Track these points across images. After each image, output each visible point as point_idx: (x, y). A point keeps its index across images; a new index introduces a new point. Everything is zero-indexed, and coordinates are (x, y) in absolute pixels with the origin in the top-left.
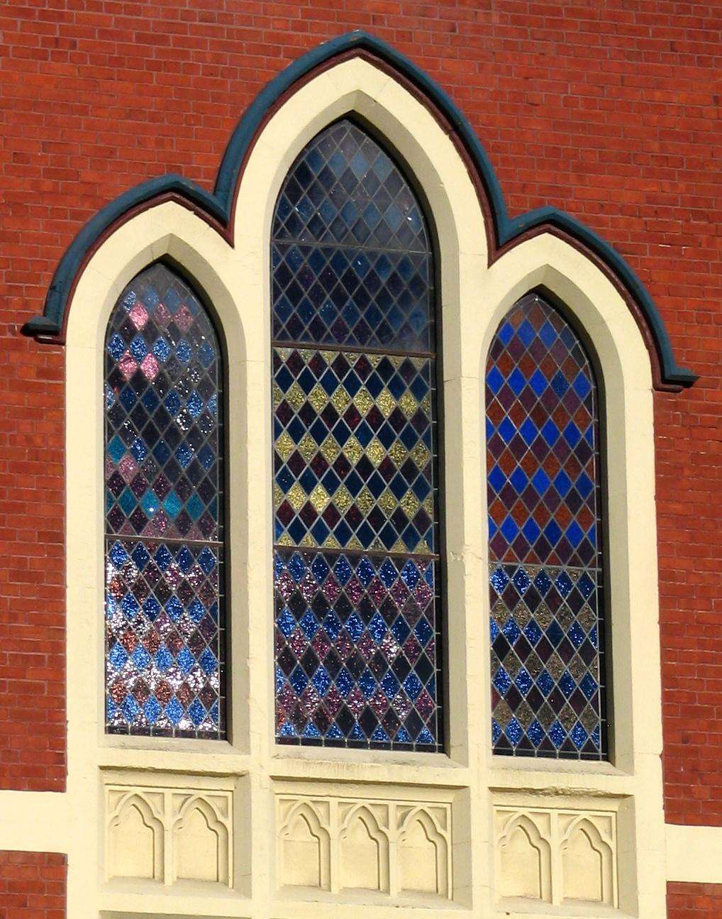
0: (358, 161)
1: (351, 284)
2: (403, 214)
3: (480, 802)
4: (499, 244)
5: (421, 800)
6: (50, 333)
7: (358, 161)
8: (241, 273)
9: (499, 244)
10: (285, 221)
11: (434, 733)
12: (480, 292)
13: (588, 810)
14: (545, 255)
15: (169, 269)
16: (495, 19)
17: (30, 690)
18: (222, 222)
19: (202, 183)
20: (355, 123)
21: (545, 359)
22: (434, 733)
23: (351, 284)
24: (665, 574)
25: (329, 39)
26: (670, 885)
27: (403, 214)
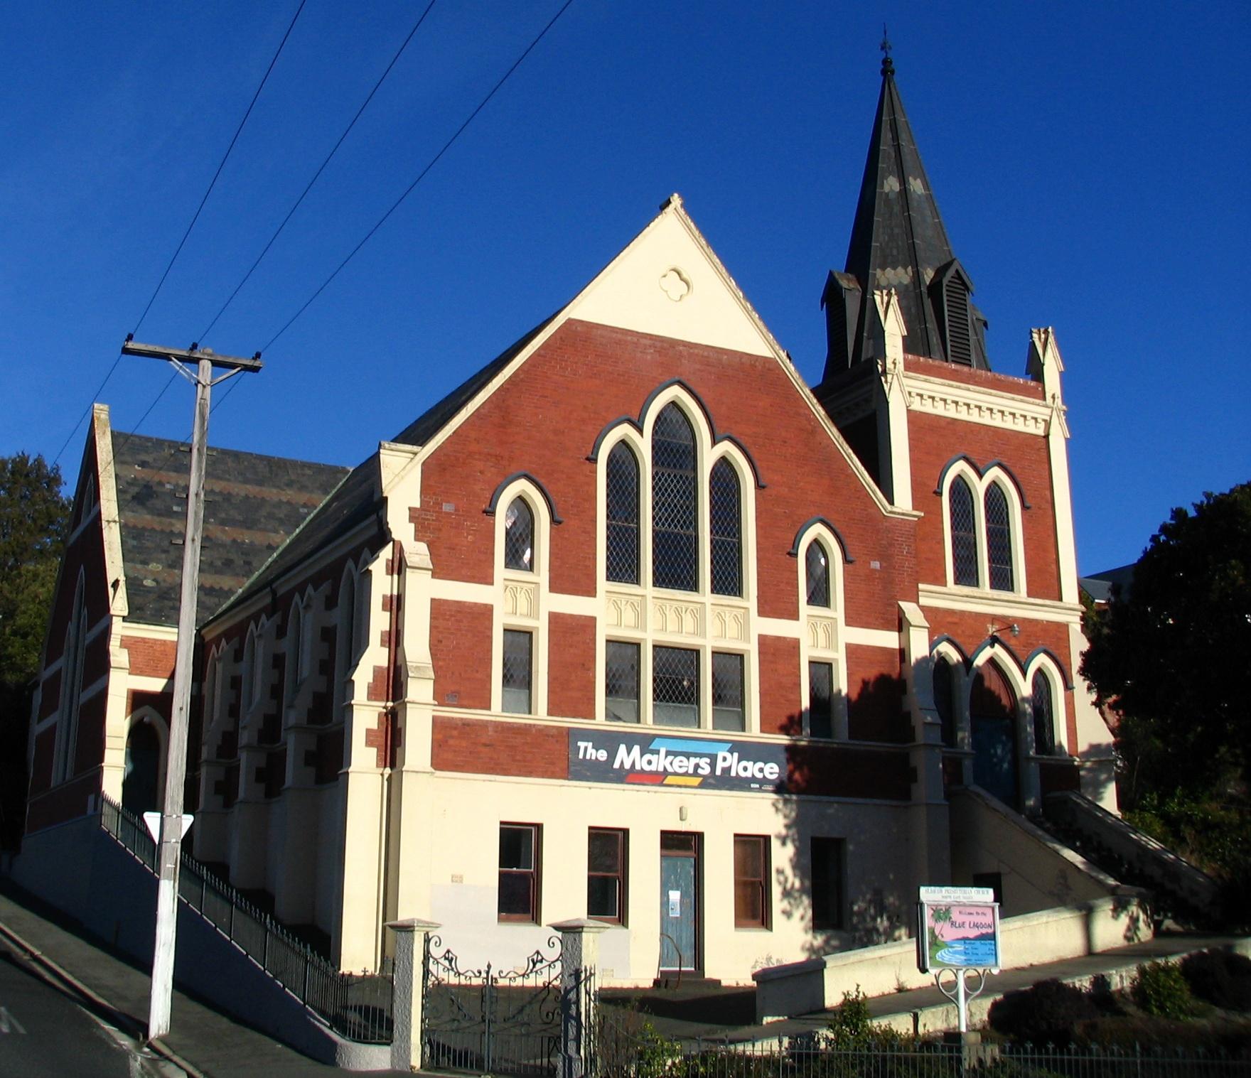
0: (675, 415)
1: (675, 450)
2: (684, 431)
3: (649, 600)
4: (714, 443)
5: (692, 606)
6: (593, 460)
7: (675, 415)
8: (644, 446)
9: (714, 442)
10: (655, 432)
11: (693, 586)
12: (708, 456)
13: (736, 611)
14: (726, 447)
15: (624, 444)
16: (230, 464)
17: (587, 567)
18: (640, 431)
19: (635, 419)
20: (674, 405)
21: (724, 475)
22: (693, 586)
23: (675, 450)
24: (758, 543)
25: (668, 380)
26: (433, 600)
27: (686, 432)
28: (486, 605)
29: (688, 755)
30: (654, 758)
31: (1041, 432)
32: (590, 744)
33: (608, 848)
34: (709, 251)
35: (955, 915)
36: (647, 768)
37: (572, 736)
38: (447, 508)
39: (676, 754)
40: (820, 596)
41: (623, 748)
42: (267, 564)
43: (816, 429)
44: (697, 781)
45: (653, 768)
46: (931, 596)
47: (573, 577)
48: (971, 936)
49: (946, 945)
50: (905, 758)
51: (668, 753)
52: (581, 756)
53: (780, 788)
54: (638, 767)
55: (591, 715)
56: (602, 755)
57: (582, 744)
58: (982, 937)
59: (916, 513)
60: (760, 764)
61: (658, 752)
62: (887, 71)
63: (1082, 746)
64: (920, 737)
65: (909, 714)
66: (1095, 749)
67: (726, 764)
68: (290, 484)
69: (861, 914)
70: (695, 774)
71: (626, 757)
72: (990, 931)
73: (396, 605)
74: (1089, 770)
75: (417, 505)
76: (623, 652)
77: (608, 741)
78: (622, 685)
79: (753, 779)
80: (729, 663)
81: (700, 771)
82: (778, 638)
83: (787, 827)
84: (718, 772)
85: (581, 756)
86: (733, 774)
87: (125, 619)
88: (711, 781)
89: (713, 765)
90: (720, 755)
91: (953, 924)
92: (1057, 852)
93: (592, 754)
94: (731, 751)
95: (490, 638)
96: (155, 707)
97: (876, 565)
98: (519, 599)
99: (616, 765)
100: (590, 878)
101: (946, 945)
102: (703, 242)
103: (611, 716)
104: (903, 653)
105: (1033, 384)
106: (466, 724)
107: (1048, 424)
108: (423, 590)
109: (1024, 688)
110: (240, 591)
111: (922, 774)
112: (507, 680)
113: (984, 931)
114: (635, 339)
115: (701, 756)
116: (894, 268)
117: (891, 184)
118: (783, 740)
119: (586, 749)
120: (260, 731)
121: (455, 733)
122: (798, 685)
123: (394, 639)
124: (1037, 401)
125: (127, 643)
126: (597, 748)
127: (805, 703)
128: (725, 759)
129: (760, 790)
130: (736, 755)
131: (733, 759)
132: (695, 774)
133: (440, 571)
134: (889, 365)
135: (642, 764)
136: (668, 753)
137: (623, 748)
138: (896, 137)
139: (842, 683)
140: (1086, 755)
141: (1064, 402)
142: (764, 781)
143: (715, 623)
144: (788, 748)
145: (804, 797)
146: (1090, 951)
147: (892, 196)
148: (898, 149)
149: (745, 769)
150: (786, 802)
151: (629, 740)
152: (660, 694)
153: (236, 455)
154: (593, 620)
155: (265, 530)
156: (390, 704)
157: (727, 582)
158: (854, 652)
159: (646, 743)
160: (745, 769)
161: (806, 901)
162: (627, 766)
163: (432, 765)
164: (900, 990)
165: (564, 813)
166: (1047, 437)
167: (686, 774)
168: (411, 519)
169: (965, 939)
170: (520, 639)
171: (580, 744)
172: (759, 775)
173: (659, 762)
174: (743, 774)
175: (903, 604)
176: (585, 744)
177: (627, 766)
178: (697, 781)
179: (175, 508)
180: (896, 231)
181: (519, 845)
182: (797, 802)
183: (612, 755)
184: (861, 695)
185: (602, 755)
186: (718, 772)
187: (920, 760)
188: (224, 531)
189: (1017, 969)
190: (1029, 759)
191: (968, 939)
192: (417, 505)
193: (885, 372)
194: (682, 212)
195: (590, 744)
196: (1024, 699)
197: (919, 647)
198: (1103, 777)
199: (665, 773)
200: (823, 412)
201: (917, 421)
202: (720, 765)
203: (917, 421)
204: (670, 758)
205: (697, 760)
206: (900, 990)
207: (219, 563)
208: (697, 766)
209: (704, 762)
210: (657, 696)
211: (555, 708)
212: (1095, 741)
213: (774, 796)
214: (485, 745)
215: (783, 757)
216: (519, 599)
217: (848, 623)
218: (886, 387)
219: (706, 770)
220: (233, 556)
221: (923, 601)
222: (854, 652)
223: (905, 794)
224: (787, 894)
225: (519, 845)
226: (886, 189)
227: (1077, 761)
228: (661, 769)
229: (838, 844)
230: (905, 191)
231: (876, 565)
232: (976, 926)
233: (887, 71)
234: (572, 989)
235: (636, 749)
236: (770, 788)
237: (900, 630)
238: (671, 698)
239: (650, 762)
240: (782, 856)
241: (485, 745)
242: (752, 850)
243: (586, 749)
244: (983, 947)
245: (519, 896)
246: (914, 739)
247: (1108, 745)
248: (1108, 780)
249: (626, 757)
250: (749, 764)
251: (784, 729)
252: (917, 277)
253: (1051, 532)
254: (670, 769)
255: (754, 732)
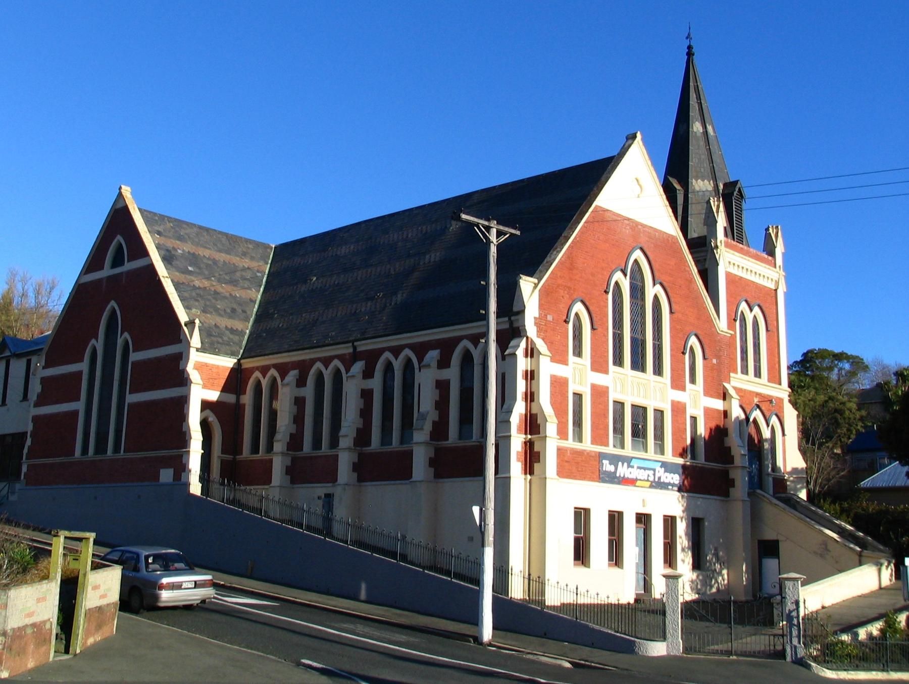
28: (602, 387)
29: (645, 469)
31: (773, 287)
34: (652, 169)
37: (601, 456)
41: (620, 463)
42: (254, 312)
43: (691, 281)
44: (648, 484)
47: (599, 366)
50: (726, 473)
51: (639, 468)
53: (680, 490)
55: (607, 445)
57: (604, 462)
62: (690, 54)
63: (789, 469)
64: (738, 461)
65: (729, 448)
66: (795, 471)
68: (244, 254)
69: (710, 562)
70: (648, 480)
73: (531, 376)
74: (792, 482)
77: (615, 460)
79: (669, 484)
83: (683, 512)
87: (198, 350)
92: (821, 531)
95: (608, 405)
96: (212, 410)
98: (579, 374)
102: (650, 163)
104: (726, 414)
105: (770, 258)
107: (777, 283)
108: (547, 369)
109: (766, 434)
110: (248, 331)
111: (738, 483)
112: (615, 430)
116: (703, 181)
117: (697, 127)
118: (681, 461)
120: (355, 439)
123: (531, 397)
125: (199, 367)
127: (689, 442)
129: (672, 490)
134: (719, 244)
137: (620, 463)
138: (699, 97)
139: (702, 430)
140: (790, 473)
141: (784, 271)
142: (673, 485)
143: (629, 386)
144: (684, 467)
145: (691, 494)
146: (880, 588)
147: (699, 134)
148: (700, 104)
150: (683, 496)
153: (207, 230)
155: (244, 288)
156: (529, 437)
158: (708, 412)
159: (628, 460)
161: (690, 554)
163: (558, 474)
164: (823, 607)
166: (776, 290)
175: (725, 384)
179: (190, 268)
180: (703, 157)
182: (688, 497)
184: (710, 436)
188: (222, 287)
189: (860, 596)
190: (768, 474)
193: (717, 247)
194: (641, 143)
196: (766, 440)
197: (737, 413)
198: (799, 486)
200: (696, 270)
201: (728, 275)
202: (657, 475)
203: (728, 275)
206: (823, 607)
207: (228, 311)
209: (651, 472)
211: (594, 441)
212: (795, 466)
213: (678, 494)
215: (681, 471)
216: (579, 374)
218: (717, 257)
219: (651, 479)
220: (235, 306)
222: (708, 412)
223: (726, 494)
224: (683, 550)
226: (695, 129)
227: (787, 476)
230: (706, 132)
233: (690, 54)
236: (676, 488)
237: (724, 399)
240: (681, 528)
242: (670, 523)
246: (733, 463)
247: (802, 469)
248: (802, 488)
249: (623, 470)
251: (682, 455)
252: (716, 186)
255: (669, 456)
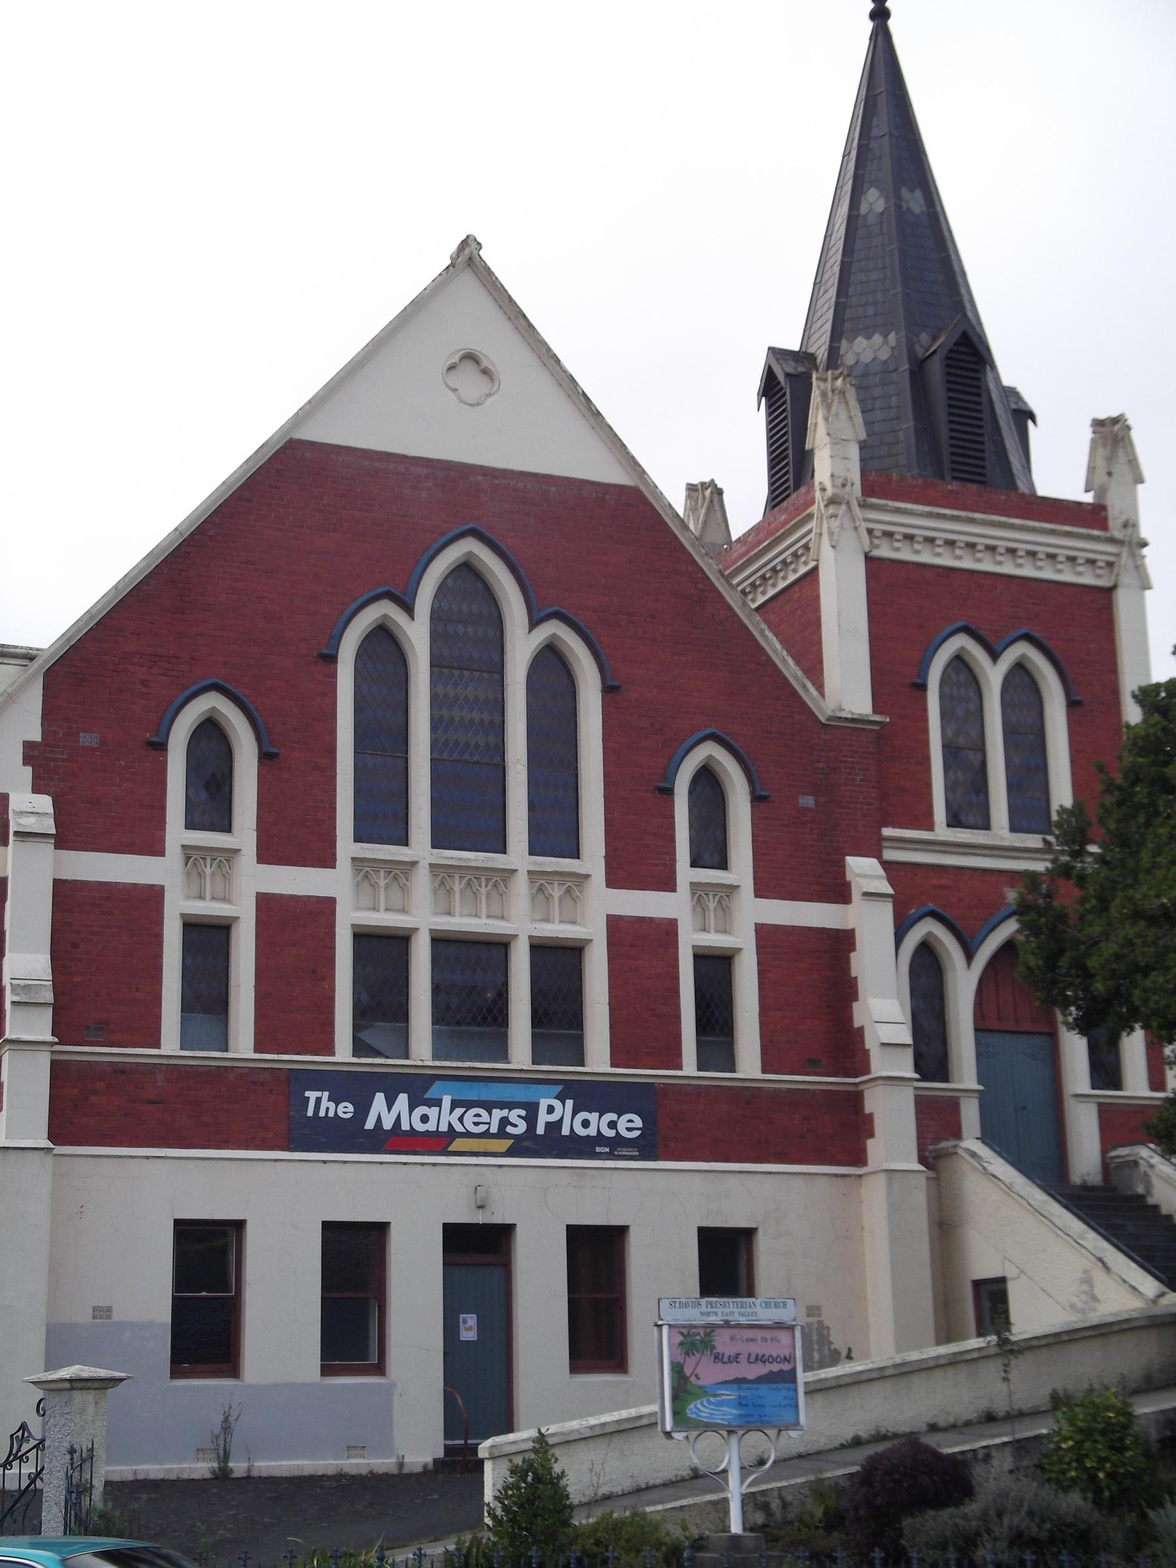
9: (534, 624)
12: (521, 646)
18: (409, 609)
29: (489, 1106)
30: (432, 1112)
32: (326, 1094)
33: (353, 1258)
35: (723, 1343)
36: (420, 1127)
38: (87, 739)
39: (468, 1105)
40: (711, 850)
41: (379, 1099)
45: (431, 1126)
46: (906, 845)
47: (295, 834)
48: (751, 1377)
49: (703, 1392)
50: (854, 1099)
52: (310, 1113)
54: (405, 1126)
56: (346, 1110)
57: (312, 1095)
58: (769, 1378)
59: (877, 718)
60: (611, 1116)
61: (438, 1103)
64: (880, 1065)
67: (554, 1117)
70: (502, 1134)
71: (383, 1112)
72: (787, 1367)
75: (37, 737)
76: (383, 951)
78: (382, 1004)
79: (600, 1138)
80: (558, 963)
81: (509, 1129)
82: (641, 920)
84: (540, 1130)
85: (310, 1113)
86: (565, 1131)
88: (528, 1143)
89: (531, 1119)
90: (544, 1104)
91: (718, 1358)
93: (328, 1107)
94: (562, 1098)
97: (808, 801)
99: (370, 1124)
100: (174, 1298)
101: (703, 1392)
103: (360, 1047)
106: (120, 1071)
113: (775, 1367)
114: (402, 468)
115: (511, 1106)
119: (319, 1100)
121: (100, 1085)
122: (674, 992)
124: (1096, 533)
126: (336, 1099)
128: (551, 1109)
130: (570, 1103)
131: (564, 1110)
132: (502, 1134)
133: (67, 836)
135: (412, 1121)
136: (455, 1105)
137: (379, 1099)
149: (586, 1124)
151: (392, 1085)
152: (444, 1013)
154: (331, 902)
157: (555, 832)
159: (418, 1088)
160: (586, 1124)
162: (387, 1125)
165: (282, 1203)
167: (486, 1135)
168: (27, 760)
169: (739, 1381)
170: (208, 939)
171: (307, 1094)
172: (610, 1133)
173: (442, 1118)
174: (581, 1131)
176: (319, 1094)
177: (387, 1125)
178: (504, 1145)
181: (207, 1256)
183: (363, 1109)
185: (346, 1110)
186: (540, 1130)
187: (876, 1102)
191: (744, 1380)
192: (37, 737)
195: (326, 1094)
199: (452, 1133)
202: (543, 1118)
204: (459, 1111)
205: (505, 1113)
208: (504, 1122)
210: (440, 1015)
214: (150, 1102)
217: (759, 893)
221: (890, 855)
223: (858, 1157)
225: (207, 1256)
228: (444, 1128)
229: (743, 1238)
231: (808, 801)
232: (761, 1359)
234: (511, 1461)
235: (403, 1100)
238: (484, 1019)
239: (425, 1119)
241: (150, 1102)
243: (319, 1100)
244: (771, 1395)
245: (206, 1331)
246: (866, 1069)
249: (383, 1112)
250: (593, 1117)
253: (723, 525)
254: (459, 1128)
